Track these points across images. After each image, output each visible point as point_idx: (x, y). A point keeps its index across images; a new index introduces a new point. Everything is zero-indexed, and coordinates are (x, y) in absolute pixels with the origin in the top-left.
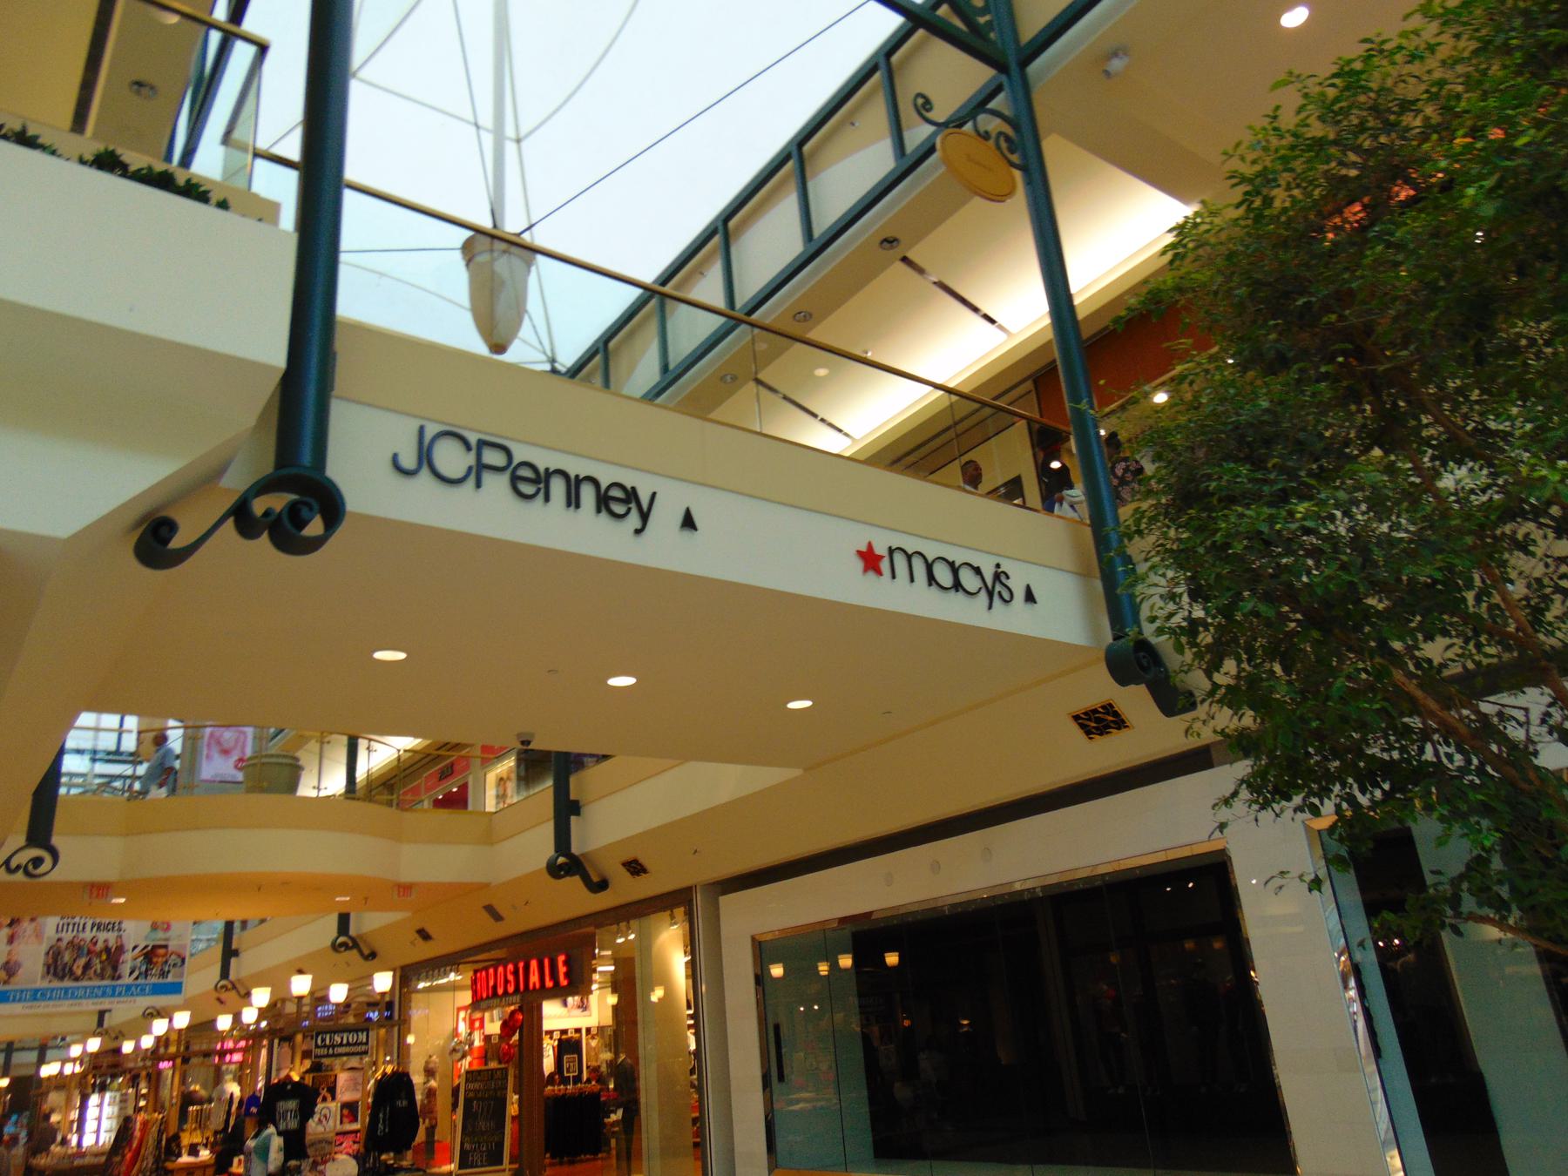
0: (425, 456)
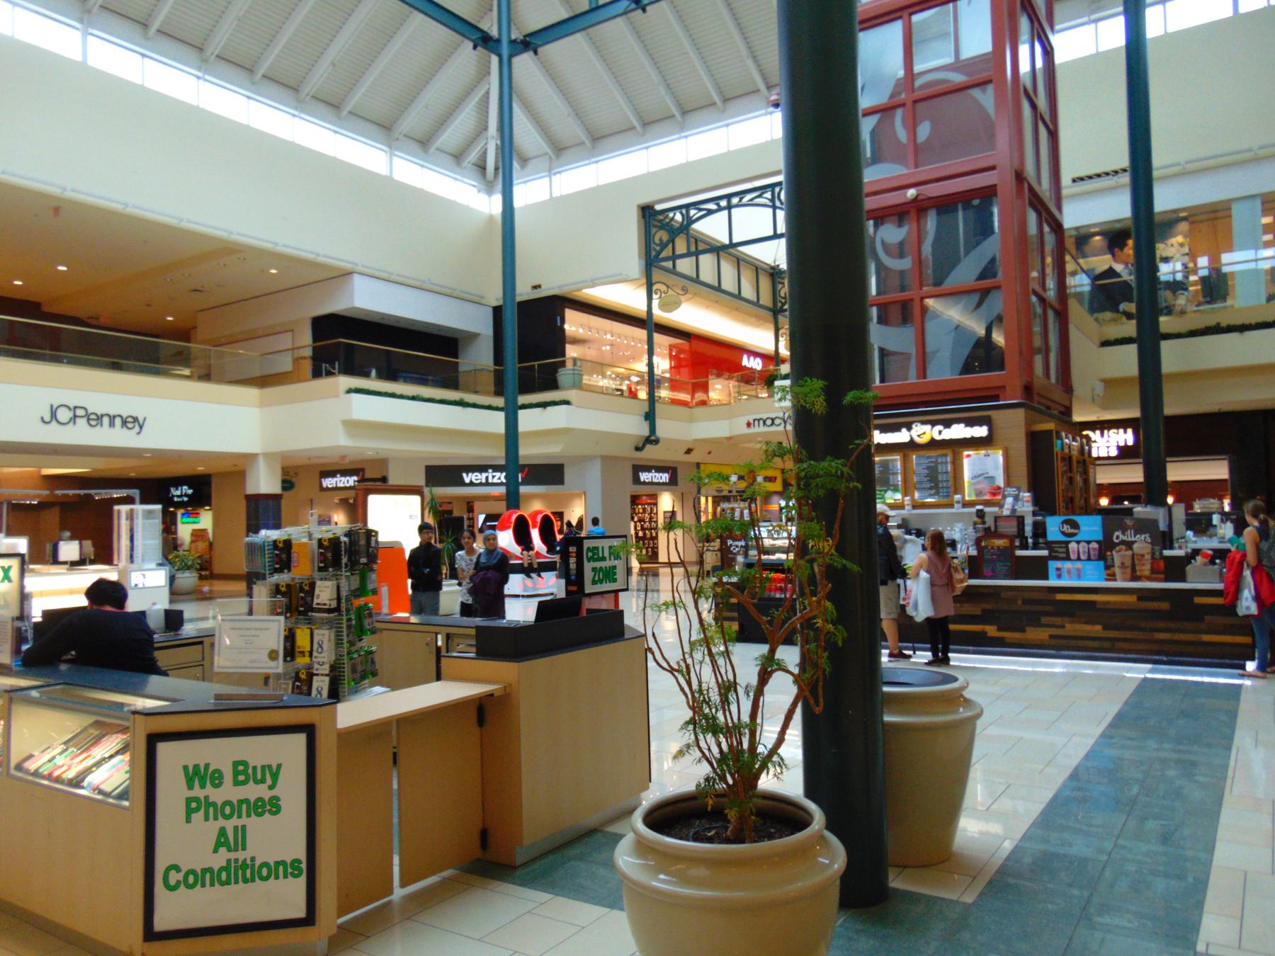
0: (53, 414)
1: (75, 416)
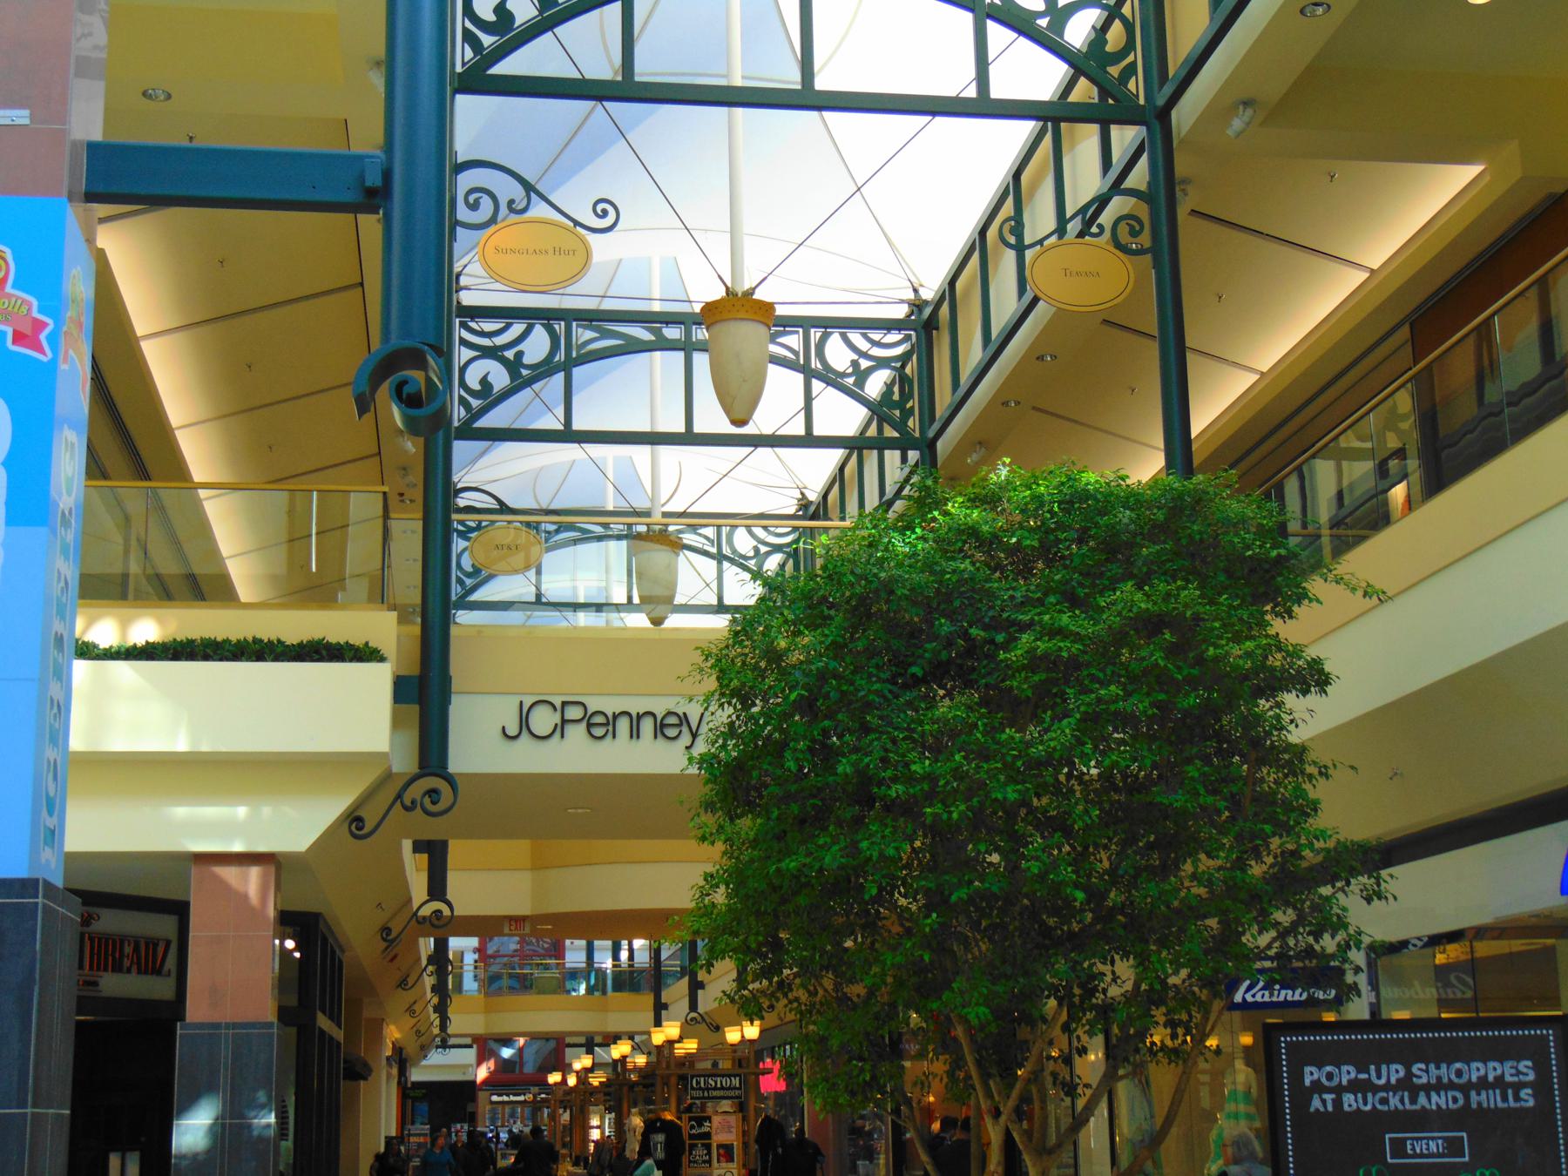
1: (564, 721)
